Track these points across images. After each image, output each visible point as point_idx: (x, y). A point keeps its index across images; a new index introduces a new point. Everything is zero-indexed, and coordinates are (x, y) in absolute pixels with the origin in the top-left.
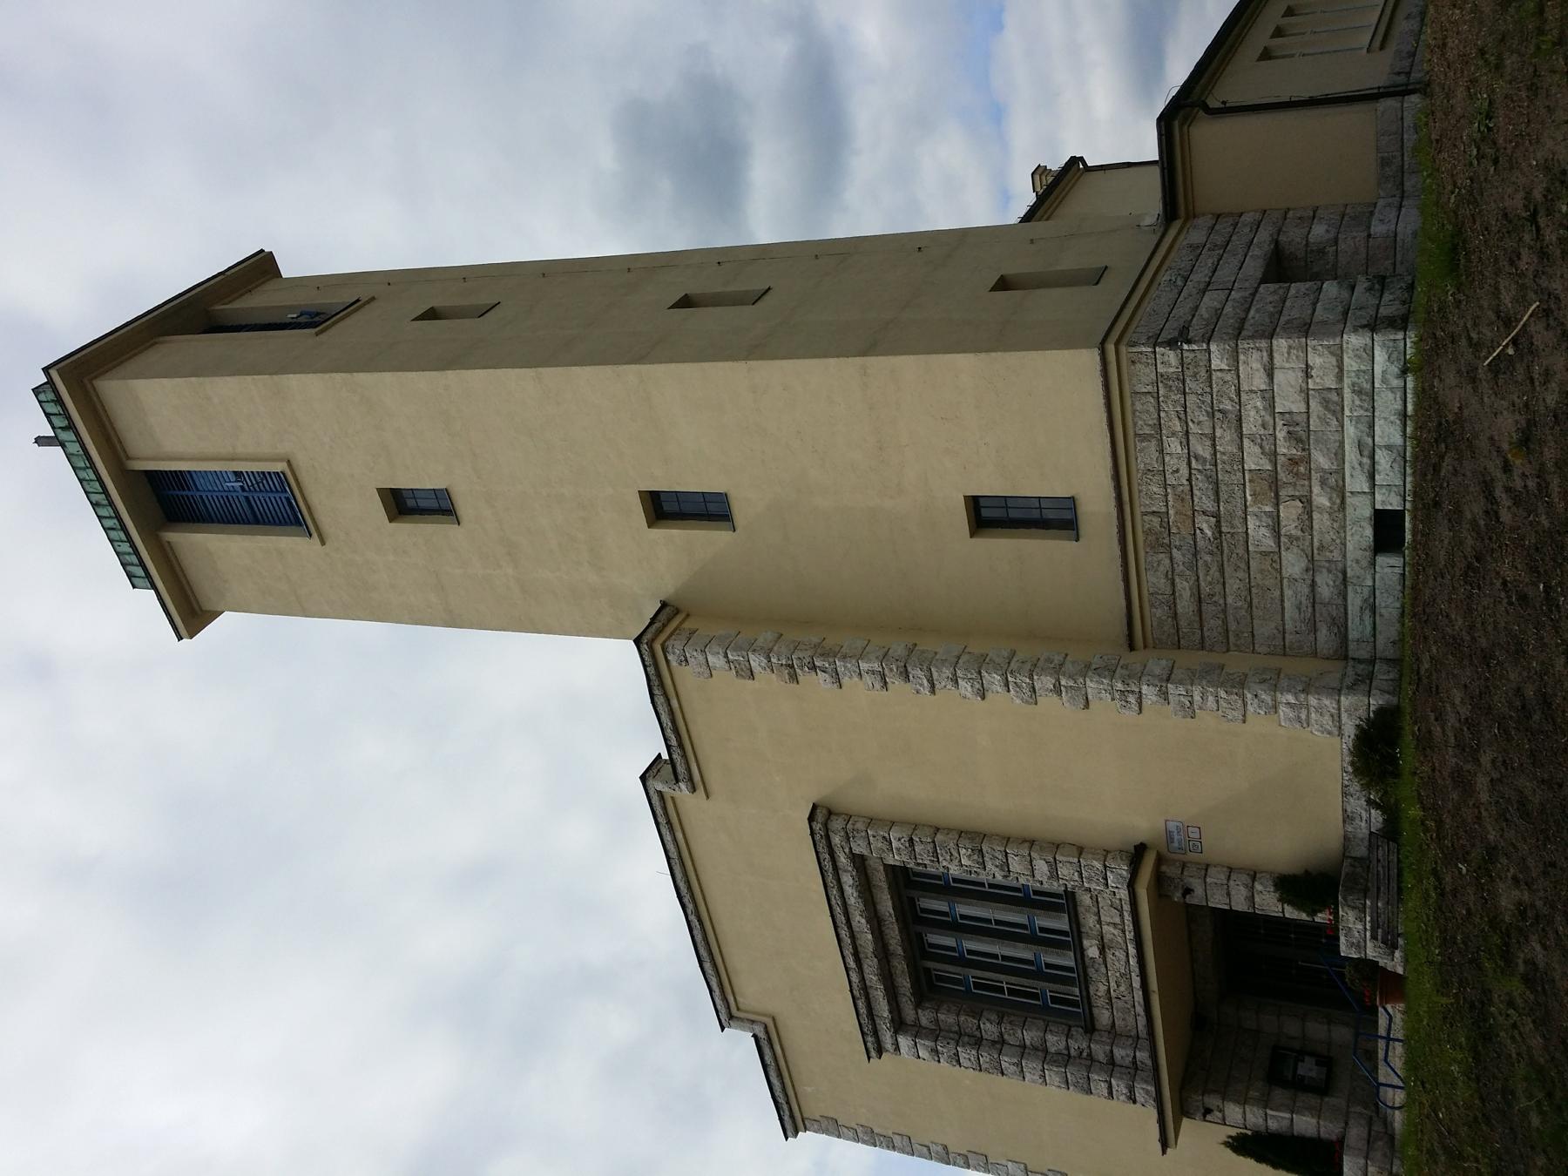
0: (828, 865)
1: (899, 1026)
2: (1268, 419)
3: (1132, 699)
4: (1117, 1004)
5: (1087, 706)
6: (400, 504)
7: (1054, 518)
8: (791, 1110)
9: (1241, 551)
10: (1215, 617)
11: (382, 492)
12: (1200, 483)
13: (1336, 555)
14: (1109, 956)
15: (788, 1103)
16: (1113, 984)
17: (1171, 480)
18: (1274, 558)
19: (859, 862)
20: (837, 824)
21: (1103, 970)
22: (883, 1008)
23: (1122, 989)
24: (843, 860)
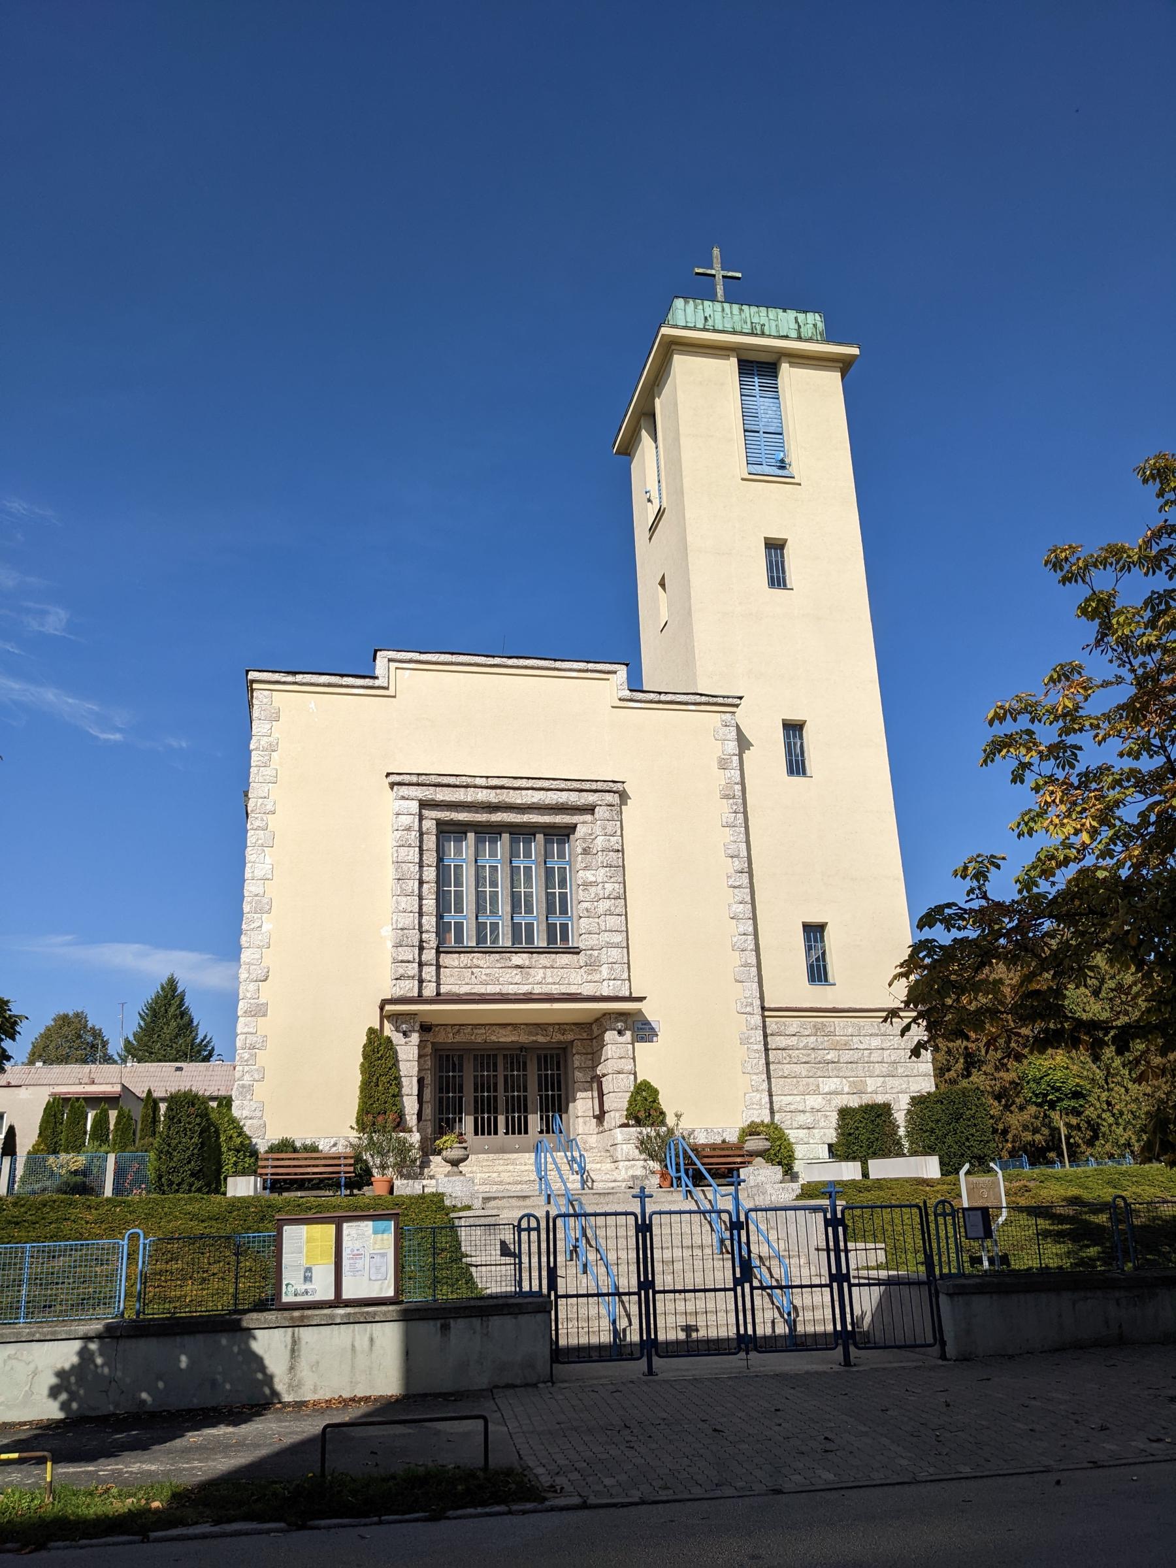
0: (587, 786)
1: (424, 804)
2: (895, 1090)
3: (748, 1009)
4: (467, 972)
5: (737, 981)
6: (775, 547)
7: (818, 972)
8: (284, 683)
9: (819, 1073)
10: (447, 1033)
11: (786, 541)
12: (856, 1055)
13: (822, 1124)
14: (515, 971)
15: (295, 683)
16: (488, 971)
17: (855, 1039)
18: (816, 1092)
19: (590, 809)
20: (615, 799)
21: (499, 965)
22: (442, 795)
23: (484, 977)
24: (591, 798)
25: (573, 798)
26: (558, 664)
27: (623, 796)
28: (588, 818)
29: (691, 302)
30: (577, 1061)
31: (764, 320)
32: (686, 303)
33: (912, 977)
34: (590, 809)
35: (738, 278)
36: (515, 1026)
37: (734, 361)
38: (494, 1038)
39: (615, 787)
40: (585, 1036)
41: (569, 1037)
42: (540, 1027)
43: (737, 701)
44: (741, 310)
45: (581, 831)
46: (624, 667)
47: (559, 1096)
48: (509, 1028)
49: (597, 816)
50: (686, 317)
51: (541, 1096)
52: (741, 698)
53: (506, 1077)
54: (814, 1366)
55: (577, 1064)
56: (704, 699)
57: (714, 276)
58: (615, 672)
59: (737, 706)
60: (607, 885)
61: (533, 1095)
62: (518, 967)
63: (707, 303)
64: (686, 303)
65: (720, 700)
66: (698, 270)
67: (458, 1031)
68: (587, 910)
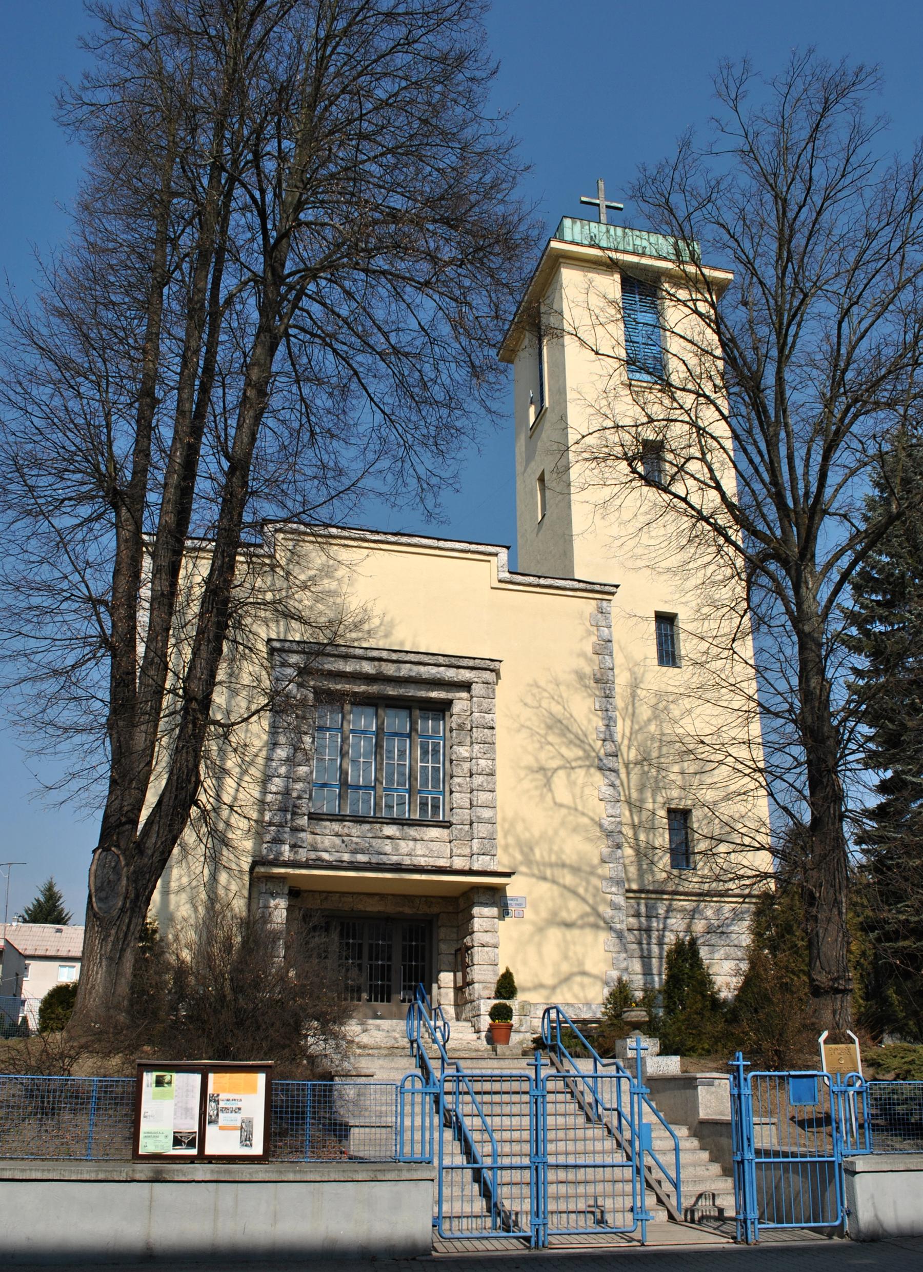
19: (466, 686)
25: (451, 674)
26: (441, 544)
27: (497, 672)
28: (464, 695)
29: (578, 222)
30: (443, 933)
31: (645, 243)
32: (574, 223)
33: (863, 611)
34: (466, 686)
35: (621, 209)
36: (382, 896)
37: (617, 277)
38: (361, 907)
39: (492, 665)
40: (451, 909)
41: (435, 910)
42: (408, 899)
43: (613, 589)
44: (625, 234)
45: (457, 708)
46: (505, 550)
47: (423, 967)
48: (377, 898)
49: (473, 693)
50: (575, 234)
51: (404, 966)
52: (617, 586)
53: (371, 946)
54: (210, 276)
55: (442, 936)
56: (582, 585)
57: (598, 205)
58: (496, 555)
59: (613, 594)
60: (480, 761)
61: (397, 964)
62: (388, 837)
63: (593, 224)
64: (574, 223)
65: (597, 588)
66: (584, 199)
67: (326, 898)
68: (460, 785)
